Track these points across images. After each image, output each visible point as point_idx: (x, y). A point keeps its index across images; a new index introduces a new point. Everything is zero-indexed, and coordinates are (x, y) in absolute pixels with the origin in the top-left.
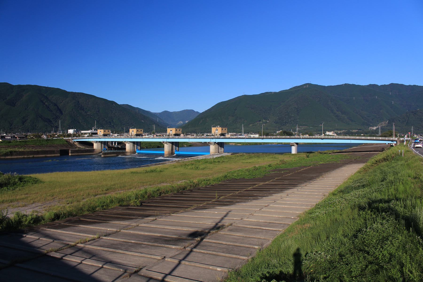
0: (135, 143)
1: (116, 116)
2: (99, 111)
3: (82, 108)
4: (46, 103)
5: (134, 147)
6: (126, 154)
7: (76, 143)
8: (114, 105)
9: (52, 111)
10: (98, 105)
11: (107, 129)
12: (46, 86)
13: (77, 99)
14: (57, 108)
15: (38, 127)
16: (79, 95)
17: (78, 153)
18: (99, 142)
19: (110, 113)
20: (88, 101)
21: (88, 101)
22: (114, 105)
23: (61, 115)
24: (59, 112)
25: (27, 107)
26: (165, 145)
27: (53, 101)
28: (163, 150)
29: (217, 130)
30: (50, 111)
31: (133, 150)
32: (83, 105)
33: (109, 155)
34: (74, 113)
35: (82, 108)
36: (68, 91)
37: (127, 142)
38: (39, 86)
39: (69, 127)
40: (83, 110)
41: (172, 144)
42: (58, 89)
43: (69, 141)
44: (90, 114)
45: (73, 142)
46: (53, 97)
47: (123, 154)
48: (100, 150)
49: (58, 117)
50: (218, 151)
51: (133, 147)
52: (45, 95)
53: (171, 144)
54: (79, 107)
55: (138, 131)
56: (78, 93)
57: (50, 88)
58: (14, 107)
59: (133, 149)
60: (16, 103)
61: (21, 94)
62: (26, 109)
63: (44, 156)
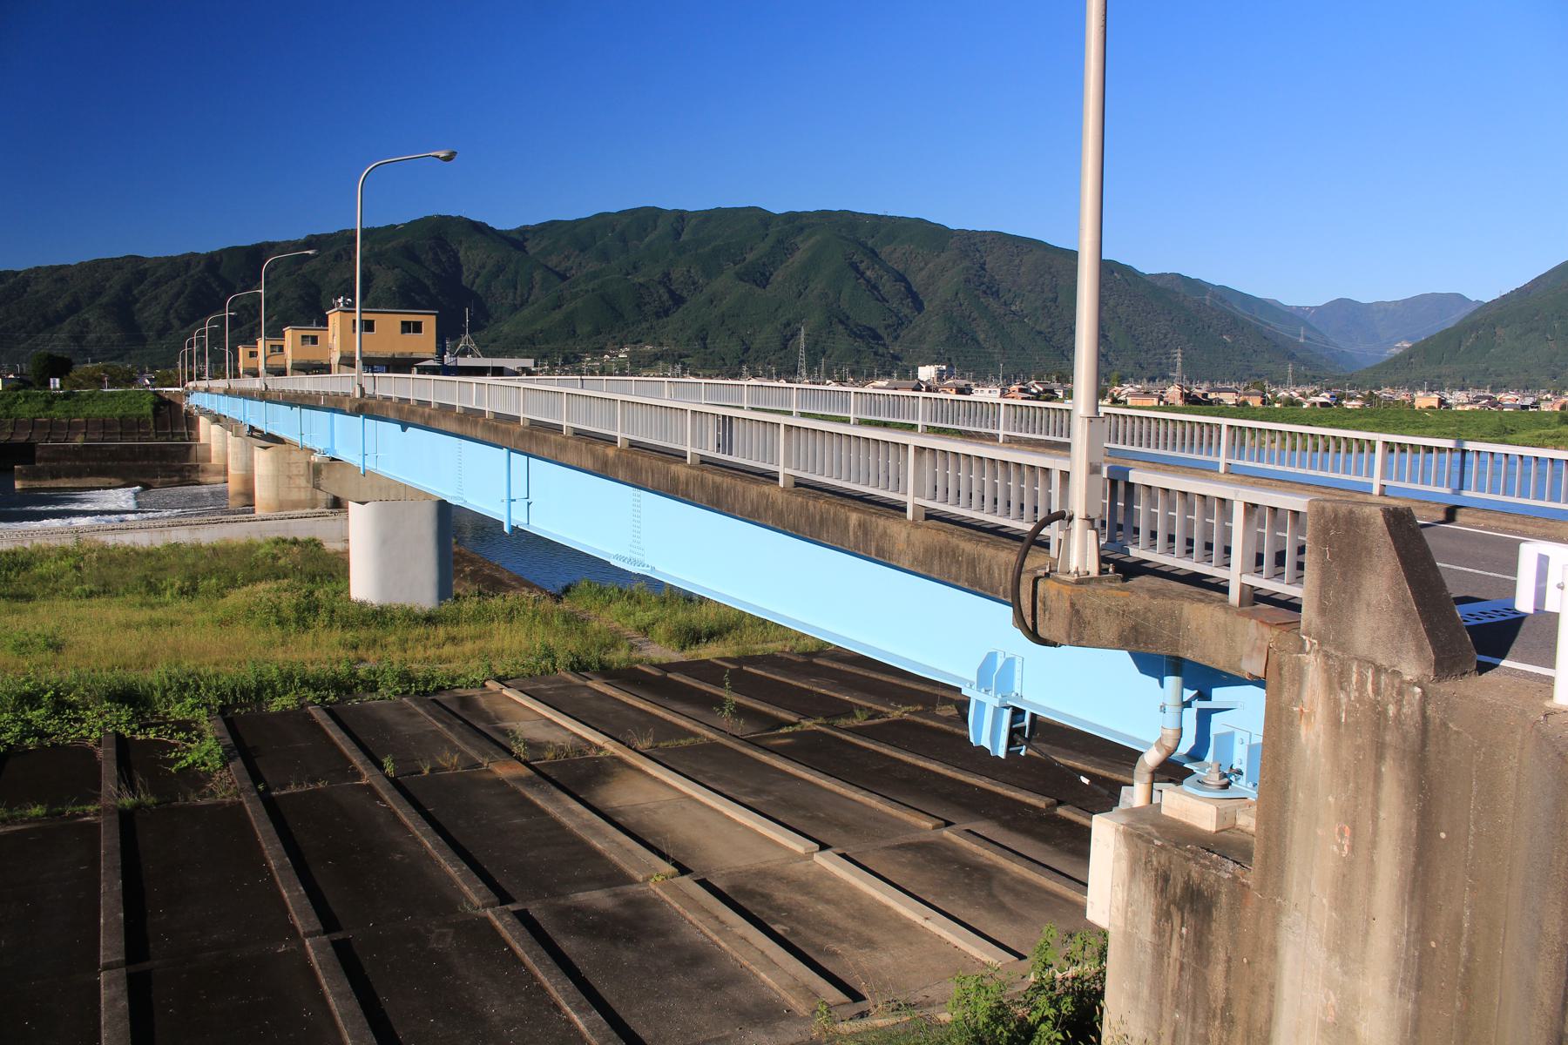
1: (1119, 317)
2: (1056, 298)
3: (994, 289)
4: (868, 273)
6: (200, 479)
10: (1054, 277)
14: (903, 289)
16: (988, 242)
20: (1017, 262)
21: (1017, 262)
22: (1116, 274)
23: (916, 313)
30: (877, 299)
32: (997, 277)
34: (961, 305)
35: (994, 289)
40: (998, 295)
46: (895, 249)
47: (176, 479)
54: (983, 284)
56: (984, 233)
58: (764, 288)
60: (771, 274)
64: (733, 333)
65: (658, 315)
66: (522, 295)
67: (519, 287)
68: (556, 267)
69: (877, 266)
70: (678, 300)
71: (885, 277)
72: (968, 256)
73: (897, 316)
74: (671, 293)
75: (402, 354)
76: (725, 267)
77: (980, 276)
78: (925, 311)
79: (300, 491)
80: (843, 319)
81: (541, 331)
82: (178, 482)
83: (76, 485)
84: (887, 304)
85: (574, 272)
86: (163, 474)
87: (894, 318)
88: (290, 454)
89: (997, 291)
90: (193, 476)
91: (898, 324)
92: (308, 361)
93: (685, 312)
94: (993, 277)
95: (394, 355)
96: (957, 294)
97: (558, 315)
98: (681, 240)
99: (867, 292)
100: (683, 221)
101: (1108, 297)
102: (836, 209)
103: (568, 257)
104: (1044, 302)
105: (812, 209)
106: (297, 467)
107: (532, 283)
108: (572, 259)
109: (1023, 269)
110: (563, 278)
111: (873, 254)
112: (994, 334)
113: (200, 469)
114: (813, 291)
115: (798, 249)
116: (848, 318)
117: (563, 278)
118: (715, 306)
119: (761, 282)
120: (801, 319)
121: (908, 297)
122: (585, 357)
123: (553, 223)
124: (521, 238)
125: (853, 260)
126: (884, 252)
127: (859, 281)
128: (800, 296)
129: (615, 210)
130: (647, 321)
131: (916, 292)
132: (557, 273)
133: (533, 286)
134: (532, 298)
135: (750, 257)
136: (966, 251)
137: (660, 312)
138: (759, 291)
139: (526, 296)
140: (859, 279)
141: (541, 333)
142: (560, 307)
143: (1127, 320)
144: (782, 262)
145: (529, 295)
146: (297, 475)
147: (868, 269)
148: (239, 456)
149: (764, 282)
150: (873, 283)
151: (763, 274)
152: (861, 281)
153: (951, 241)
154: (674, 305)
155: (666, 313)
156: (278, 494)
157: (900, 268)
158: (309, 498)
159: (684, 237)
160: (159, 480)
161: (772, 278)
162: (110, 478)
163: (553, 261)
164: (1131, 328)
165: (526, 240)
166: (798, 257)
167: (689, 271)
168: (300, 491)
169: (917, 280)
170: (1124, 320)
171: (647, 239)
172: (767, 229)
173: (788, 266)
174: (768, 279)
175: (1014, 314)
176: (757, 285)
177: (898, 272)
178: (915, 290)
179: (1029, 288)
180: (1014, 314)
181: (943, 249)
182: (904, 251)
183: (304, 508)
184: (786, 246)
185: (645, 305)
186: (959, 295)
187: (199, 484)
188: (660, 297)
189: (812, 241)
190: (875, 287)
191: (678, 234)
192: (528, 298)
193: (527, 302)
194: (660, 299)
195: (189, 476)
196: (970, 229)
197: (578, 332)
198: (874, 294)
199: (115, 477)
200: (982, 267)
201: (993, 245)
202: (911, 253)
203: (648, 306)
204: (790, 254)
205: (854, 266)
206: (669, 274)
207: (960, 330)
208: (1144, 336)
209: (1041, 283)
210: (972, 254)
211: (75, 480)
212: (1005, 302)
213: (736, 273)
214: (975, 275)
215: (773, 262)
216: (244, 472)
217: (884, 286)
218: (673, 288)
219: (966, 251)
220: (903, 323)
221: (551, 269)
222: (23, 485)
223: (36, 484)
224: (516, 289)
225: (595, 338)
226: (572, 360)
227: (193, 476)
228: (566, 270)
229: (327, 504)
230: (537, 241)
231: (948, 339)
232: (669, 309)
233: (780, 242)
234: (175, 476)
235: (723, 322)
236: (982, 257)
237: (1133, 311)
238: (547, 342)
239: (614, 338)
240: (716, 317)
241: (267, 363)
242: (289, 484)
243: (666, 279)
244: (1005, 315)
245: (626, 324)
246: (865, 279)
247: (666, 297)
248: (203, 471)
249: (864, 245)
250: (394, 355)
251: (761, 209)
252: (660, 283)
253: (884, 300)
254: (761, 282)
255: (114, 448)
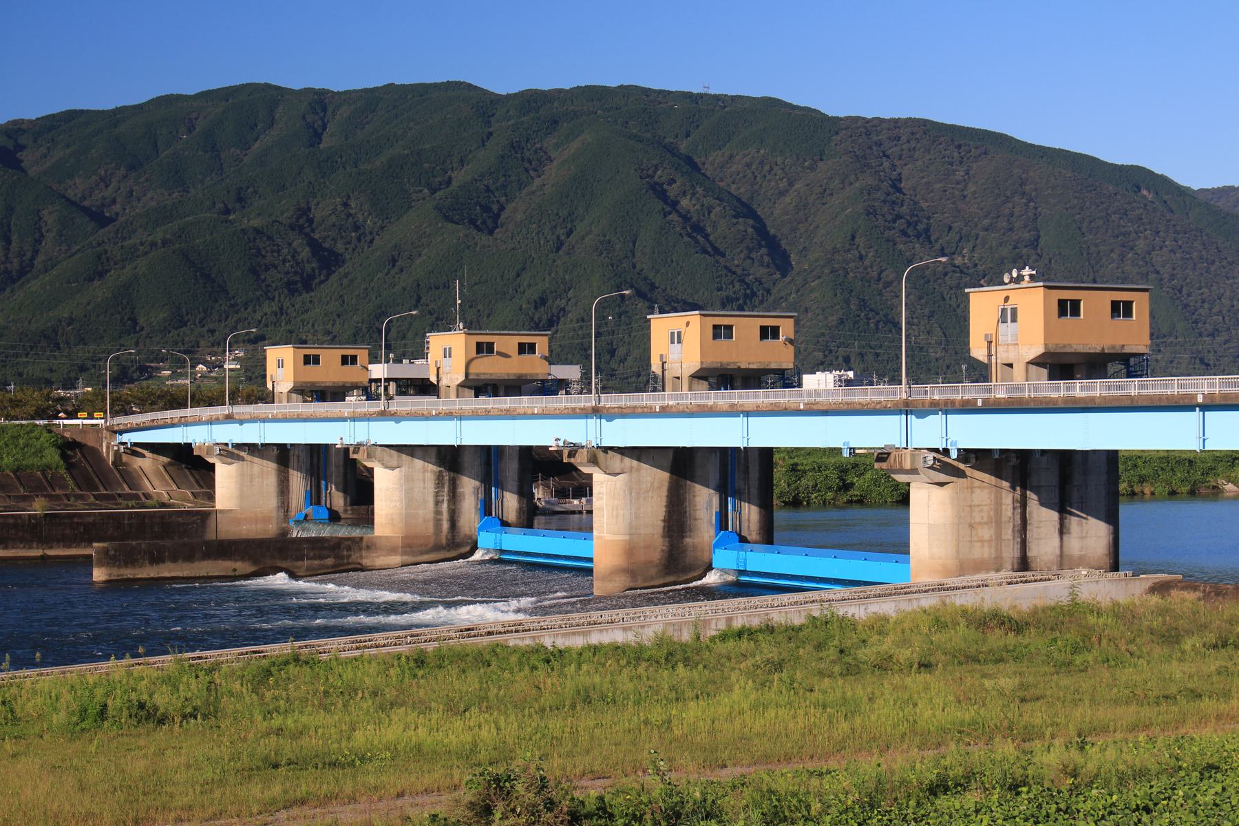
0: (467, 459)
1: (1157, 272)
2: (1037, 240)
3: (920, 227)
4: (685, 203)
5: (454, 497)
6: (366, 562)
7: (147, 463)
8: (1150, 197)
9: (723, 255)
10: (1030, 200)
11: (333, 340)
12: (695, 91)
13: (886, 164)
14: (750, 230)
15: (623, 360)
16: (904, 138)
17: (46, 541)
18: (979, 458)
19: (1114, 256)
20: (960, 174)
21: (960, 174)
22: (1145, 192)
23: (778, 276)
24: (766, 259)
25: (569, 234)
26: (595, 476)
27: (733, 187)
28: (587, 528)
29: (1014, 320)
30: (704, 251)
31: (438, 522)
32: (924, 205)
33: (169, 565)
34: (861, 258)
35: (920, 227)
36: (831, 113)
37: (599, 454)
38: (647, 92)
39: (825, 356)
40: (929, 237)
41: (278, 463)
42: (771, 105)
43: (90, 443)
44: (976, 265)
45: (117, 452)
46: (731, 156)
47: (330, 561)
48: (266, 520)
49: (759, 293)
50: (1011, 552)
51: (437, 494)
52: (684, 146)
53: (665, 476)
54: (899, 217)
55: (484, 349)
56: (896, 123)
57: (717, 98)
58: (491, 232)
59: (438, 513)
60: (502, 208)
61: (538, 146)
62: (562, 244)
63: (36, 552)
64: (438, 319)
65: (292, 289)
66: (21, 254)
67: (15, 237)
68: (84, 198)
69: (700, 190)
70: (329, 260)
71: (718, 209)
72: (867, 165)
73: (742, 281)
74: (315, 246)
75: (1113, 347)
76: (414, 196)
77: (894, 202)
78: (794, 272)
79: (983, 546)
80: (644, 288)
81: (71, 321)
82: (333, 566)
83: (186, 573)
84: (721, 260)
85: (117, 208)
86: (311, 554)
87: (737, 285)
88: (972, 492)
89: (927, 230)
90: (355, 557)
91: (746, 296)
92: (721, 363)
93: (345, 282)
94: (916, 203)
95: (1103, 349)
96: (853, 238)
97: (100, 291)
98: (321, 146)
99: (686, 239)
100: (325, 110)
101: (1133, 235)
102: (613, 83)
103: (105, 181)
104: (1015, 248)
105: (567, 86)
106: (981, 511)
107: (40, 229)
108: (114, 184)
109: (972, 188)
110: (100, 218)
111: (691, 165)
112: (927, 311)
113: (364, 543)
114: (583, 238)
115: (550, 160)
116: (653, 287)
117: (100, 218)
118: (402, 271)
119: (484, 222)
120: (566, 292)
121: (760, 246)
122: (159, 369)
123: (71, 115)
124: (10, 145)
125: (656, 178)
126: (711, 162)
127: (670, 217)
128: (558, 249)
129: (191, 91)
130: (273, 299)
131: (775, 236)
132: (86, 211)
133: (42, 236)
134: (41, 258)
135: (460, 177)
136: (864, 157)
137: (296, 283)
138: (483, 239)
139: (29, 254)
140: (670, 213)
141: (69, 324)
142: (101, 275)
143: (1173, 277)
144: (521, 186)
145: (36, 252)
146: (980, 523)
147: (684, 194)
148: (621, 512)
149: (490, 223)
150: (694, 219)
151: (486, 209)
152: (673, 217)
153: (837, 138)
154: (321, 269)
155: (308, 284)
156: (958, 552)
157: (742, 191)
158: (993, 556)
159: (327, 142)
160: (306, 563)
161: (504, 216)
162: (236, 560)
163: (76, 187)
164: (1180, 291)
165: (22, 148)
166: (553, 175)
167: (346, 205)
168: (983, 546)
169: (776, 214)
170: (1166, 277)
171: (257, 145)
172: (488, 123)
173: (533, 192)
174: (498, 216)
175: (962, 272)
176: (479, 229)
177: (739, 200)
178: (772, 232)
179: (986, 222)
180: (962, 272)
181: (822, 153)
182: (747, 159)
183: (988, 571)
184: (527, 154)
185: (267, 269)
186: (857, 240)
187: (363, 569)
188: (295, 254)
189: (575, 145)
190: (698, 229)
191: (317, 136)
192: (32, 259)
193: (32, 265)
194: (293, 257)
195: (349, 557)
196: (869, 117)
197: (141, 321)
198: (697, 242)
199: (243, 559)
200: (896, 186)
201: (913, 144)
202: (762, 163)
203: (273, 272)
204: (535, 170)
205: (659, 191)
206: (309, 209)
207: (863, 304)
208: (1206, 305)
209: (1007, 211)
210: (874, 162)
211: (184, 565)
212: (943, 249)
213: (438, 208)
214: (884, 202)
215: (504, 187)
216: (627, 537)
217: (715, 227)
218: (317, 236)
219: (864, 157)
220: (754, 294)
221: (74, 203)
222: (110, 575)
223: (128, 573)
224: (9, 241)
225: (174, 332)
226: (135, 376)
227: (355, 557)
228: (103, 205)
229: (1013, 565)
230: (43, 150)
231: (842, 322)
232: (312, 277)
233: (514, 147)
234: (329, 557)
235: (419, 299)
236: (893, 168)
237: (1182, 259)
238: (82, 341)
239: (212, 331)
240: (404, 289)
241: (471, 370)
242: (971, 536)
243: (303, 221)
244: (946, 274)
245: (232, 306)
246: (680, 215)
247: (305, 253)
248: (368, 548)
249: (671, 150)
250: (1103, 349)
251: (470, 85)
252: (292, 228)
253: (717, 251)
254: (484, 222)
255: (91, 519)
